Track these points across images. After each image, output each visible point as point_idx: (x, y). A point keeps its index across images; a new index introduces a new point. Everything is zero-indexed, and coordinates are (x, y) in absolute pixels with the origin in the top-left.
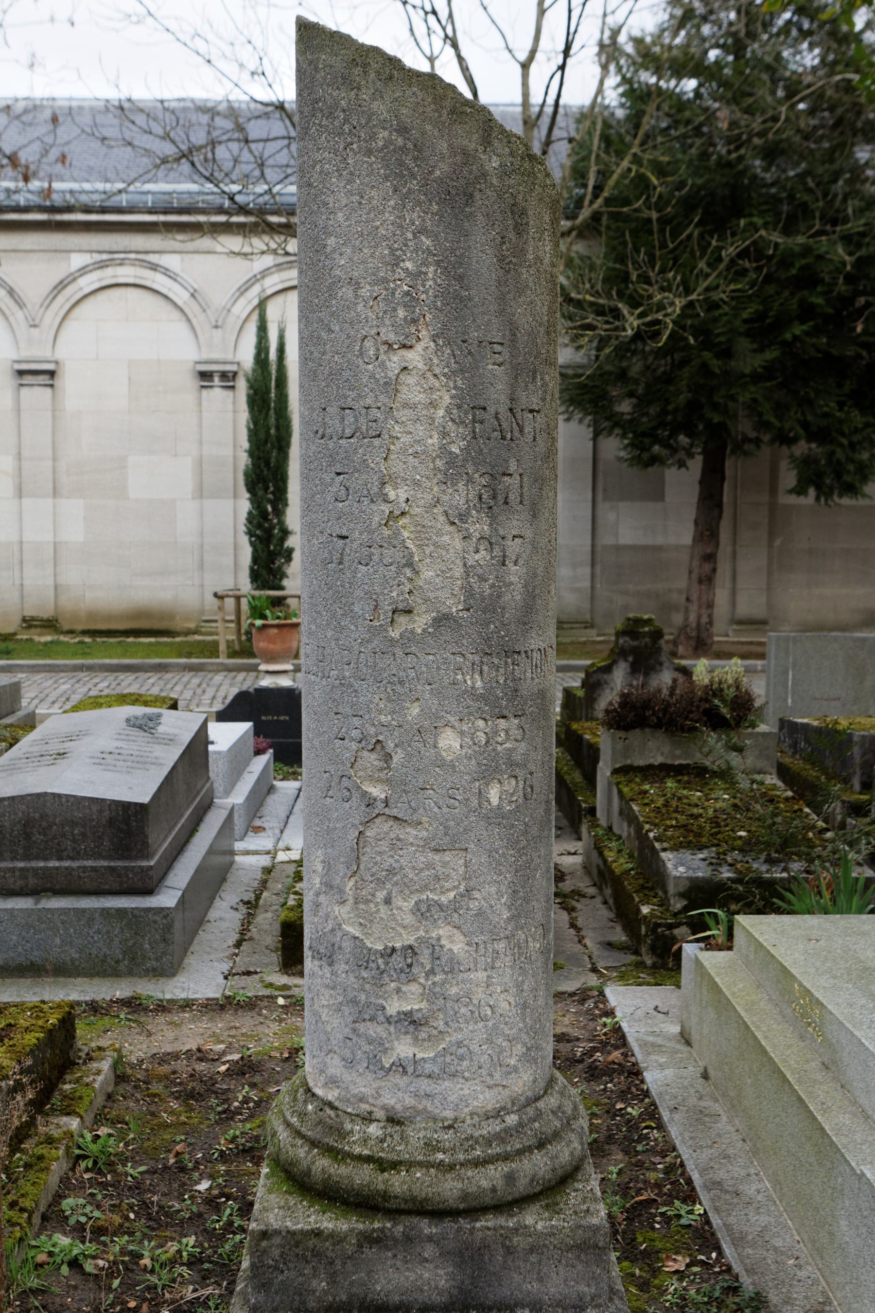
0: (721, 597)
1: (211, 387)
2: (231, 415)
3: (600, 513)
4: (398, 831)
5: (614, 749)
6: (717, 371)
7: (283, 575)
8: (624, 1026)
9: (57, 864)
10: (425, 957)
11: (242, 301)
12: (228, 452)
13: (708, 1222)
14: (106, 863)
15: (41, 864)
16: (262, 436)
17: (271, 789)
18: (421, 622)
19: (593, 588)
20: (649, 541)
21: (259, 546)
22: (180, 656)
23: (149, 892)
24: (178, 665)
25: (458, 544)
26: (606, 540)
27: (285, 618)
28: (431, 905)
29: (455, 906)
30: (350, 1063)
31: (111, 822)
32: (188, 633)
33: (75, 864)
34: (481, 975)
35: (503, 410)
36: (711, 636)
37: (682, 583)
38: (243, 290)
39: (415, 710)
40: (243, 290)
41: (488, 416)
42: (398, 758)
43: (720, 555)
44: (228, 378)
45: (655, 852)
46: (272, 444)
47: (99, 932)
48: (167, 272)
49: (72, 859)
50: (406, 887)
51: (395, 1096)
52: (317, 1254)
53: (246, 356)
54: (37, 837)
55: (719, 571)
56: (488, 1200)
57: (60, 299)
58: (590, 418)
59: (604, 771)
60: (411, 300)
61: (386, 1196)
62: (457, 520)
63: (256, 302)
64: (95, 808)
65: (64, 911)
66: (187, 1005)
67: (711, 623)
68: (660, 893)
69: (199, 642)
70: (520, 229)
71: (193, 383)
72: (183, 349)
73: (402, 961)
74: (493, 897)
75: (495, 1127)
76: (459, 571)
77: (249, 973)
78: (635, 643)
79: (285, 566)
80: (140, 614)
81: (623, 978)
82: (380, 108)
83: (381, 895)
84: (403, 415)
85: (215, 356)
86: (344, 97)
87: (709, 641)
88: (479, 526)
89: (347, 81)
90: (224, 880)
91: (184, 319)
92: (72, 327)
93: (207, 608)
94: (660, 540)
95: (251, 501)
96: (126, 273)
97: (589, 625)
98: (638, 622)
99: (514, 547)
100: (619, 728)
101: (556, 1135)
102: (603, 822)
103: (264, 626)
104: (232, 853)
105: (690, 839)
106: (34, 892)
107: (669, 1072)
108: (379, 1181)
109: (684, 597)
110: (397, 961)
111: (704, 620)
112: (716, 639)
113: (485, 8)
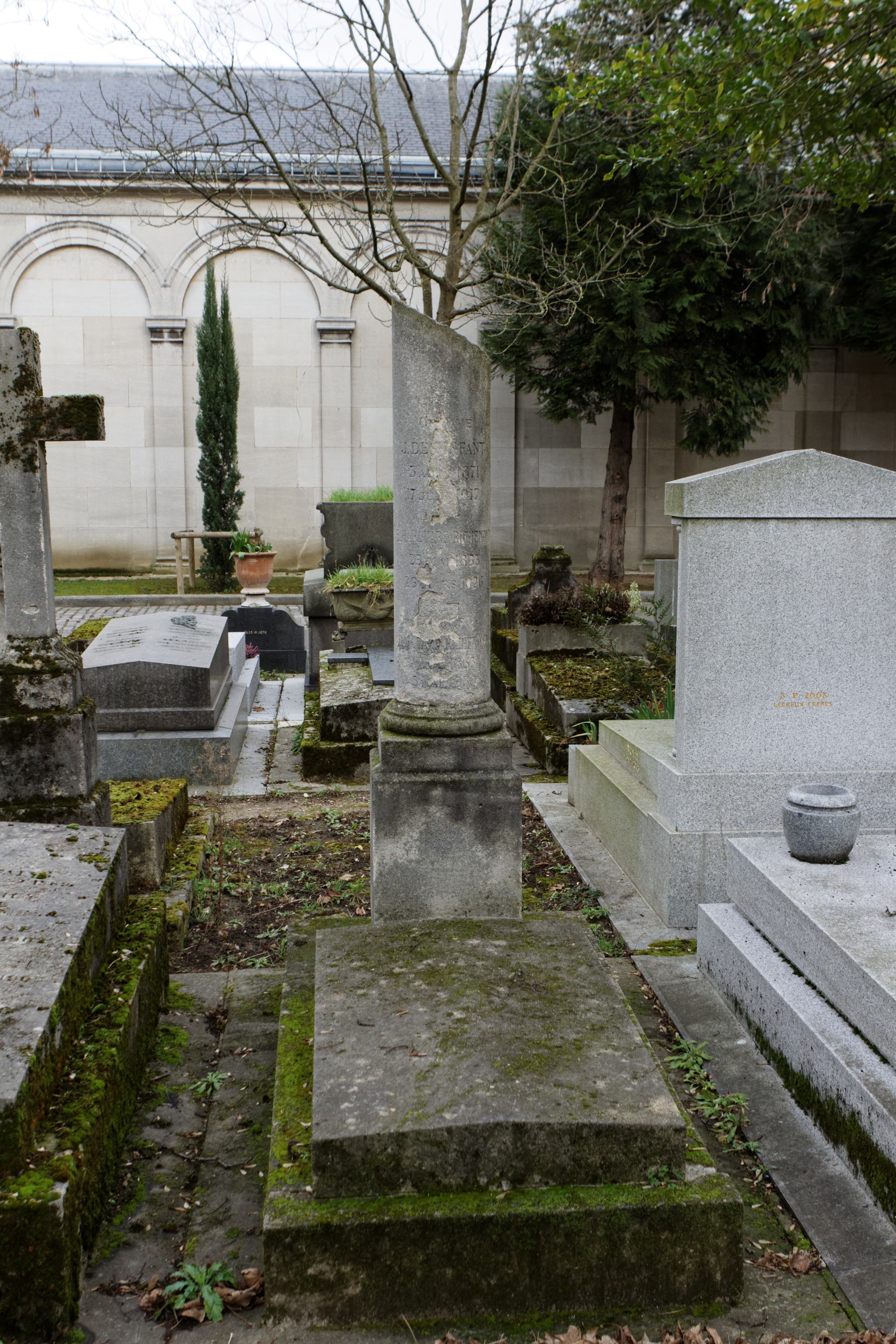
0: (632, 534)
1: (161, 342)
2: (180, 368)
3: (521, 458)
4: (434, 597)
5: (528, 639)
6: (622, 338)
7: (235, 517)
8: (532, 799)
9: (147, 710)
10: (444, 643)
11: (189, 262)
12: (178, 403)
13: (576, 871)
14: (181, 709)
15: (137, 710)
16: (213, 389)
17: (259, 686)
18: (442, 520)
19: (516, 527)
20: (567, 484)
21: (212, 491)
22: (139, 592)
23: (211, 728)
24: (141, 599)
25: (455, 492)
26: (528, 483)
27: (263, 550)
28: (446, 623)
29: (455, 624)
30: (415, 686)
31: (185, 681)
32: (143, 572)
33: (160, 710)
34: (464, 651)
35: (471, 444)
36: (623, 570)
37: (595, 522)
38: (190, 251)
39: (440, 552)
40: (190, 251)
41: (466, 446)
42: (434, 570)
43: (630, 497)
44: (177, 334)
45: (555, 701)
46: (222, 397)
47: (179, 755)
48: (117, 234)
49: (156, 706)
50: (437, 617)
51: (433, 695)
52: (406, 751)
53: (195, 313)
54: (134, 692)
55: (630, 511)
56: (468, 731)
57: (17, 259)
58: (510, 373)
59: (521, 655)
60: (438, 405)
61: (431, 730)
62: (455, 483)
63: (204, 260)
64: (173, 672)
65: (155, 741)
66: (243, 799)
67: (622, 558)
68: (559, 728)
69: (154, 579)
70: (476, 378)
71: (144, 338)
72: (134, 307)
73: (435, 645)
74: (469, 621)
75: (470, 708)
76: (455, 502)
77: (281, 782)
78: (549, 569)
79: (236, 509)
80: (98, 554)
81: (532, 779)
82: (427, 337)
83: (427, 621)
84: (436, 445)
85: (165, 313)
86: (414, 332)
87: (620, 575)
88: (463, 485)
89: (415, 326)
90: (245, 737)
91: (134, 278)
92: (29, 287)
93: (160, 548)
94: (576, 484)
95: (204, 449)
96: (79, 235)
97: (513, 561)
98: (551, 551)
99: (475, 493)
100: (531, 623)
101: (492, 714)
102: (521, 694)
103: (246, 557)
104: (246, 723)
105: (580, 693)
106: (132, 730)
107: (560, 818)
108: (428, 724)
109: (597, 536)
110: (434, 645)
111: (616, 555)
112: (627, 573)
113: (417, 21)
